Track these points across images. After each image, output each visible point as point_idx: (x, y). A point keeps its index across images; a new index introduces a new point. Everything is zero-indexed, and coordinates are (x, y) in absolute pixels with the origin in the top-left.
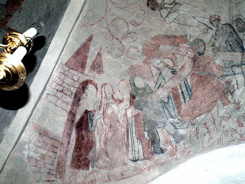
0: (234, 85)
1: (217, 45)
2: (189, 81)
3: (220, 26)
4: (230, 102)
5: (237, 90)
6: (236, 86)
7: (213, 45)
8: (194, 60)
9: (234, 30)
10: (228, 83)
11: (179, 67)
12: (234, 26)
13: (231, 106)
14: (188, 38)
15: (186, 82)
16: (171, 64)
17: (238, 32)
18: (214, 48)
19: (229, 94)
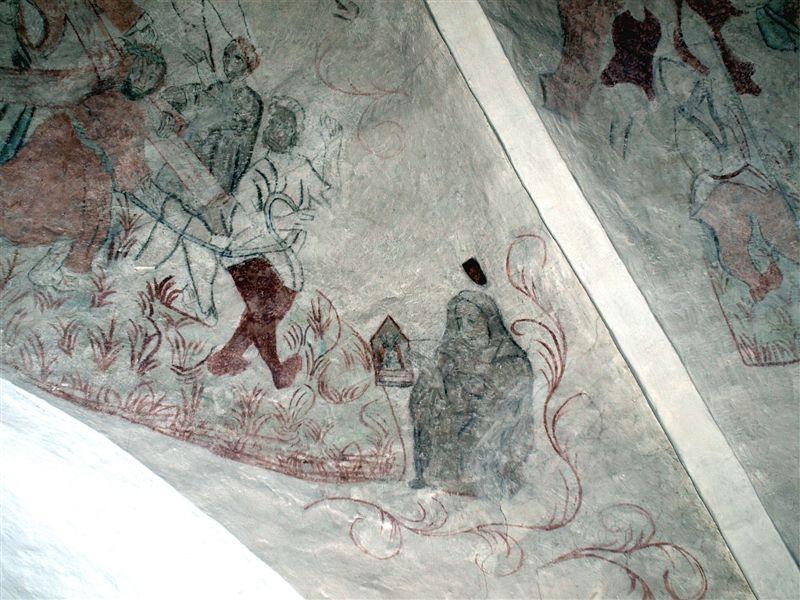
0: (134, 241)
1: (188, 114)
2: (37, 121)
3: (237, 84)
4: (89, 268)
5: (130, 259)
6: (137, 248)
7: (178, 106)
8: (100, 88)
9: (257, 124)
10: (128, 224)
11: (47, 65)
12: (267, 117)
13: (83, 282)
14: (140, 25)
15: (27, 116)
16: (34, 33)
17: (260, 139)
18: (174, 112)
19: (104, 249)
